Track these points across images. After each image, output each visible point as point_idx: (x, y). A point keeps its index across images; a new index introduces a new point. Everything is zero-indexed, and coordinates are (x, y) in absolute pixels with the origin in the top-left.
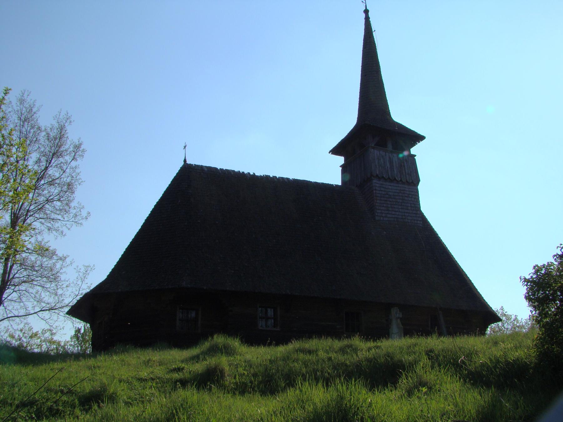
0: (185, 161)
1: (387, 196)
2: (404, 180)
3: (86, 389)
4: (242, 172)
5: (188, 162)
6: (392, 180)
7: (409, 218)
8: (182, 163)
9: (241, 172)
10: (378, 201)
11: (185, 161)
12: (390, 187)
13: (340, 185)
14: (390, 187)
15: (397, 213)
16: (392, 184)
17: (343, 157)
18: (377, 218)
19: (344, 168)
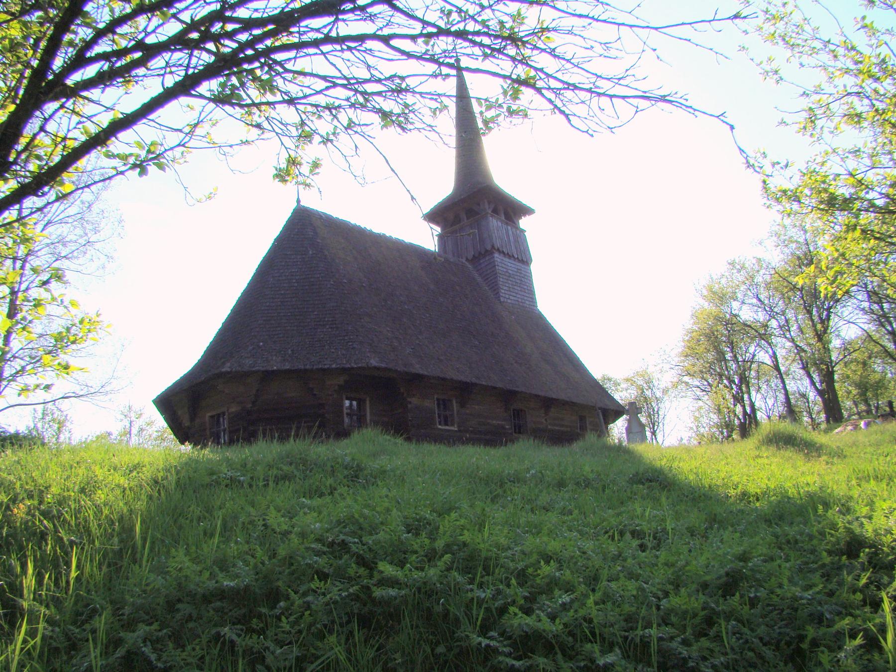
0: (298, 201)
1: (507, 274)
2: (520, 258)
3: (128, 633)
4: (74, 84)
5: (302, 203)
6: (510, 256)
7: (527, 302)
8: (294, 205)
9: (73, 86)
10: (501, 280)
11: (298, 201)
12: (509, 264)
13: (433, 249)
14: (509, 264)
15: (519, 296)
16: (510, 261)
17: (520, 221)
18: (502, 299)
19: (441, 237)
